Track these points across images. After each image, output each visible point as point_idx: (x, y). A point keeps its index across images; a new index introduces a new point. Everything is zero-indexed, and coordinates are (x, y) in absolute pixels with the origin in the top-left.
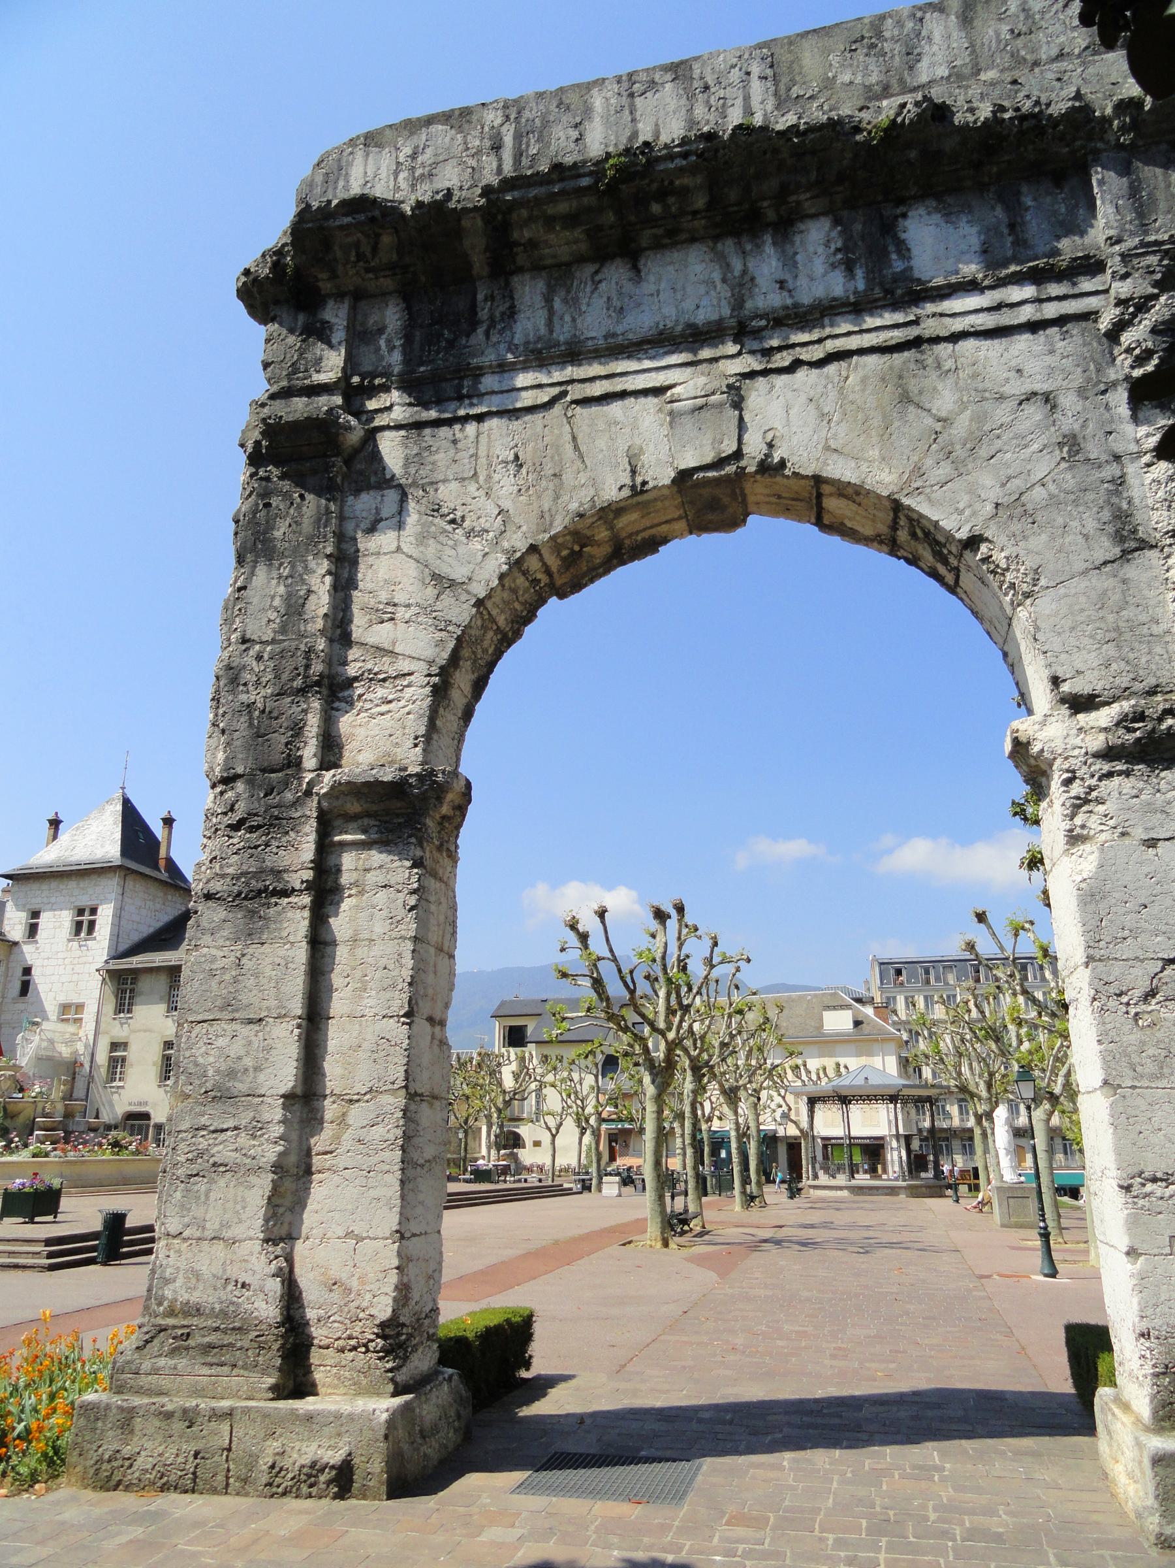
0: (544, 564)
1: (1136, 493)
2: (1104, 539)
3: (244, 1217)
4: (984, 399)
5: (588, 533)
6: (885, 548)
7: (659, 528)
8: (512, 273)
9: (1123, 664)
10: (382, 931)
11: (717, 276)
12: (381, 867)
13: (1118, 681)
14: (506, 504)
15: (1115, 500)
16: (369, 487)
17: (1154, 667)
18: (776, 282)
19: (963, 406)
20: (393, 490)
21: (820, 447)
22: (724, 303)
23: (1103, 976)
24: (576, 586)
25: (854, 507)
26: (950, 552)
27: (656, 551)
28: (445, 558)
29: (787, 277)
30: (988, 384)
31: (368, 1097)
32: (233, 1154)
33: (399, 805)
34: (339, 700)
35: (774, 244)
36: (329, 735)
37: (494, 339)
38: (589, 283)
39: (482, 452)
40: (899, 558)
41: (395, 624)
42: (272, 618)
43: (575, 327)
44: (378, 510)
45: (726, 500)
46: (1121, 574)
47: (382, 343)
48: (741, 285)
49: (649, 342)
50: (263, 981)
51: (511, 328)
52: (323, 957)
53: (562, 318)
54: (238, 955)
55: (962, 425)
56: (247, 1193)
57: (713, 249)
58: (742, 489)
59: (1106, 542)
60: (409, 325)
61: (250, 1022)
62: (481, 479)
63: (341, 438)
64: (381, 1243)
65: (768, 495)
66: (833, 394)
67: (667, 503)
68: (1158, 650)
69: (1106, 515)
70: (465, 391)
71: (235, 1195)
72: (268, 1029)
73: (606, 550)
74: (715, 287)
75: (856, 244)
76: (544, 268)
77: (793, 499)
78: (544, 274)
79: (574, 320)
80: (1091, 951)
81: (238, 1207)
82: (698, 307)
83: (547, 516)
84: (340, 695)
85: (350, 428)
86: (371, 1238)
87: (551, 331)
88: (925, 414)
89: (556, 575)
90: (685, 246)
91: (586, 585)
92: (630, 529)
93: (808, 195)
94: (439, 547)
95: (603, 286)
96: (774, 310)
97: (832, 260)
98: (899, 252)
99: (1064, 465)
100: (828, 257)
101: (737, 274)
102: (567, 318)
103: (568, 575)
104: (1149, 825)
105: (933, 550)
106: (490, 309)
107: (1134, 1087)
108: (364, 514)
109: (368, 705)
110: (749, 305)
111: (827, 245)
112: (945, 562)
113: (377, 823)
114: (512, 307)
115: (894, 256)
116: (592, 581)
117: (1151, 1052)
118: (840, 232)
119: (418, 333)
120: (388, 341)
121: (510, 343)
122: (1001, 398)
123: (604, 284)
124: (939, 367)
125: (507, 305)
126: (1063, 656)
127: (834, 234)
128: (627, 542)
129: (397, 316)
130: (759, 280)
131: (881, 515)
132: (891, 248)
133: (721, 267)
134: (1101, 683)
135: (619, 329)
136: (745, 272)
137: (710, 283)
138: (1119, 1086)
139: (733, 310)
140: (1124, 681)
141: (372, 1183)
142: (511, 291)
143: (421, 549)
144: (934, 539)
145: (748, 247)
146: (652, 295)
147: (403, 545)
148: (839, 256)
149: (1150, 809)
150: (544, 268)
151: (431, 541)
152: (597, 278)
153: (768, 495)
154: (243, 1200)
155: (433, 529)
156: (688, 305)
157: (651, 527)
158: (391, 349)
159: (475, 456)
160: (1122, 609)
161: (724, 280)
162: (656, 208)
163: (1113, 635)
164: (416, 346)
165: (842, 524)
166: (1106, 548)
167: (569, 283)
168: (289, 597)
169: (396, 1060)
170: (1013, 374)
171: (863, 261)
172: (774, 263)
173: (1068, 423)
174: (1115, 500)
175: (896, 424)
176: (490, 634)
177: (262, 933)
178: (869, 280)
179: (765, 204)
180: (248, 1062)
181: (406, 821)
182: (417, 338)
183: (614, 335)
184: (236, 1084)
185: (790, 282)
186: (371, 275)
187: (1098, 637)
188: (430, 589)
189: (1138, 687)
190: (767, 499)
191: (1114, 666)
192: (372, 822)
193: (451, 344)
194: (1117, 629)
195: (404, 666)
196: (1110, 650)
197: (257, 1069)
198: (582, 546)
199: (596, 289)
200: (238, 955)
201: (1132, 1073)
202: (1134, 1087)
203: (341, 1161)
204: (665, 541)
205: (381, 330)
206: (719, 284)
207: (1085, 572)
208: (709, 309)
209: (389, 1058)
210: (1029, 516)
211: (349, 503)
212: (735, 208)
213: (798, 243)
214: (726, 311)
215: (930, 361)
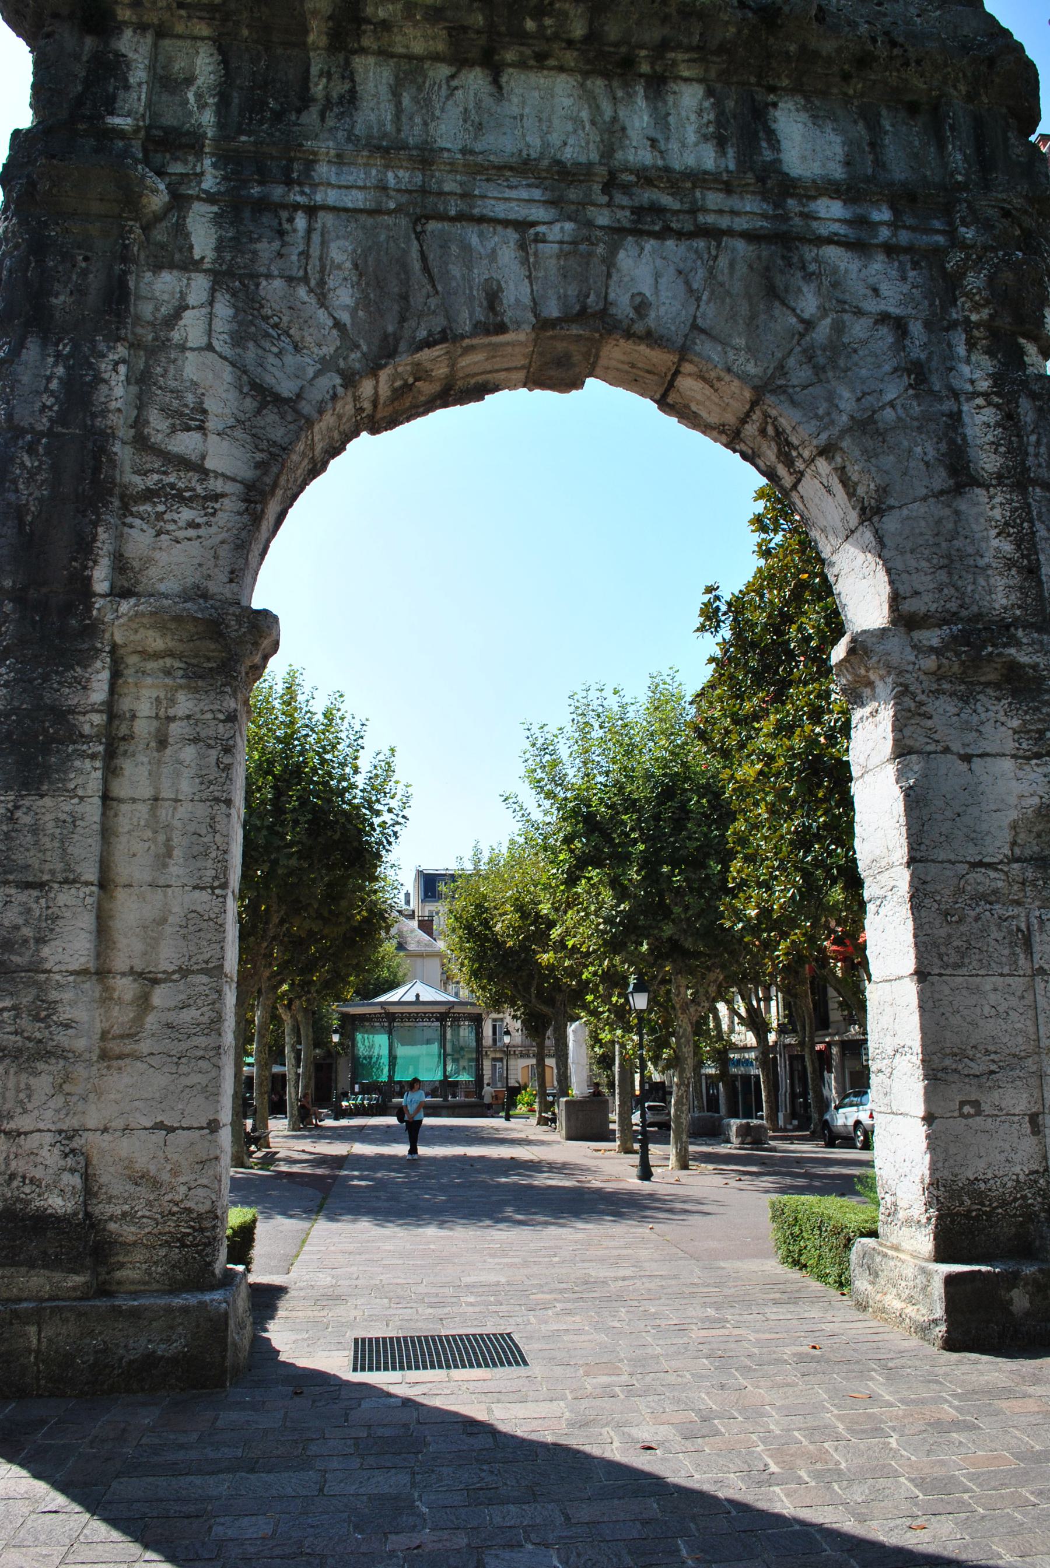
0: (376, 393)
1: (969, 431)
2: (941, 469)
3: (29, 1106)
4: (844, 311)
5: (428, 365)
6: (724, 438)
7: (495, 375)
8: (355, 52)
9: (953, 591)
10: (191, 790)
11: (585, 115)
12: (188, 717)
13: (948, 606)
14: (345, 317)
15: (952, 434)
16: (172, 266)
17: (977, 597)
18: (648, 138)
19: (824, 311)
20: (202, 275)
21: (688, 324)
22: (591, 146)
23: (922, 876)
24: (392, 423)
25: (708, 391)
26: (800, 455)
27: (480, 398)
28: (269, 367)
29: (659, 136)
30: (847, 297)
31: (175, 977)
32: (12, 1037)
33: (213, 646)
34: (132, 514)
35: (647, 97)
36: (121, 555)
37: (331, 123)
38: (444, 87)
39: (315, 251)
40: (735, 451)
41: (205, 435)
42: (48, 403)
43: (427, 132)
44: (183, 296)
45: (577, 358)
46: (954, 504)
47: (191, 96)
48: (612, 133)
49: (511, 169)
50: (45, 840)
51: (351, 115)
52: (116, 815)
53: (411, 119)
54: (10, 806)
55: (823, 330)
56: (32, 1081)
57: (582, 85)
58: (598, 350)
59: (943, 473)
60: (225, 82)
61: (28, 885)
62: (313, 283)
63: (145, 201)
64: (198, 1133)
65: (622, 362)
66: (701, 273)
67: (517, 349)
68: (982, 581)
69: (943, 447)
70: (295, 175)
71: (18, 1083)
72: (52, 895)
73: (434, 388)
74: (584, 128)
75: (728, 121)
76: (392, 56)
77: (648, 372)
78: (392, 62)
79: (425, 124)
80: (914, 854)
81: (22, 1096)
82: (565, 144)
83: (391, 340)
84: (134, 509)
85: (155, 191)
86: (184, 1129)
87: (399, 131)
88: (789, 312)
89: (380, 407)
90: (552, 73)
91: (402, 423)
92: (468, 371)
93: (686, 57)
94: (260, 351)
95: (459, 93)
96: (645, 168)
97: (704, 131)
98: (769, 141)
99: (911, 392)
100: (700, 127)
101: (607, 119)
102: (418, 120)
103: (391, 408)
104: (967, 741)
105: (779, 450)
106: (326, 87)
107: (940, 975)
108: (166, 297)
109: (171, 527)
110: (619, 155)
111: (700, 113)
112: (789, 463)
113: (182, 665)
114: (353, 91)
115: (764, 144)
116: (408, 420)
117: (955, 944)
118: (713, 104)
119: (235, 95)
120: (199, 96)
121: (350, 132)
122: (859, 312)
123: (460, 92)
124: (803, 268)
125: (347, 86)
126: (905, 576)
127: (707, 104)
128: (460, 383)
129: (210, 68)
130: (630, 132)
131: (735, 404)
132: (762, 135)
133: (590, 107)
134: (935, 605)
135: (478, 147)
136: (615, 119)
137: (577, 121)
138: (929, 974)
139: (602, 156)
140: (953, 606)
141: (182, 1069)
142: (352, 73)
143: (238, 350)
144: (786, 440)
145: (620, 94)
146: (515, 118)
147: (215, 343)
148: (711, 129)
149: (967, 727)
150: (392, 56)
151: (251, 345)
152: (454, 83)
153: (622, 362)
154: (28, 1087)
155: (253, 329)
156: (555, 139)
157: (490, 372)
158: (202, 106)
159: (305, 254)
160: (953, 539)
161: (593, 123)
162: (530, 25)
163: (946, 561)
164: (234, 109)
165: (687, 407)
166: (940, 479)
167: (420, 80)
168: (67, 383)
169: (209, 936)
170: (869, 292)
171: (734, 140)
172: (646, 118)
173: (917, 353)
174: (952, 434)
175: (763, 317)
176: (306, 461)
177: (41, 783)
178: (739, 163)
179: (643, 53)
180: (27, 932)
181: (218, 667)
182: (236, 101)
183: (472, 152)
184: (14, 958)
185: (662, 142)
186: (183, 12)
187: (935, 561)
188: (248, 400)
189: (964, 613)
190: (620, 366)
191: (946, 591)
192: (177, 664)
193: (278, 116)
194: (949, 556)
195: (217, 485)
196: (942, 576)
197: (41, 941)
198: (416, 380)
199: (452, 95)
200: (10, 806)
201: (940, 963)
202: (940, 975)
203: (145, 1047)
204: (495, 389)
205: (190, 81)
206: (588, 126)
207: (924, 499)
208: (577, 149)
209: (202, 934)
210: (881, 434)
211: (146, 280)
212: (612, 49)
213: (670, 103)
214: (594, 156)
215: (795, 260)
